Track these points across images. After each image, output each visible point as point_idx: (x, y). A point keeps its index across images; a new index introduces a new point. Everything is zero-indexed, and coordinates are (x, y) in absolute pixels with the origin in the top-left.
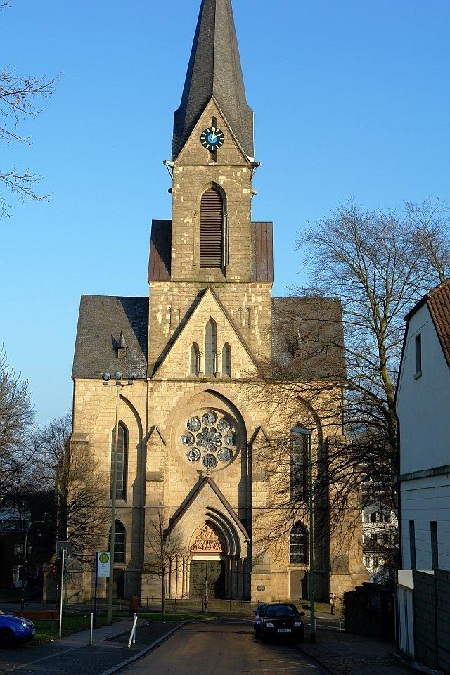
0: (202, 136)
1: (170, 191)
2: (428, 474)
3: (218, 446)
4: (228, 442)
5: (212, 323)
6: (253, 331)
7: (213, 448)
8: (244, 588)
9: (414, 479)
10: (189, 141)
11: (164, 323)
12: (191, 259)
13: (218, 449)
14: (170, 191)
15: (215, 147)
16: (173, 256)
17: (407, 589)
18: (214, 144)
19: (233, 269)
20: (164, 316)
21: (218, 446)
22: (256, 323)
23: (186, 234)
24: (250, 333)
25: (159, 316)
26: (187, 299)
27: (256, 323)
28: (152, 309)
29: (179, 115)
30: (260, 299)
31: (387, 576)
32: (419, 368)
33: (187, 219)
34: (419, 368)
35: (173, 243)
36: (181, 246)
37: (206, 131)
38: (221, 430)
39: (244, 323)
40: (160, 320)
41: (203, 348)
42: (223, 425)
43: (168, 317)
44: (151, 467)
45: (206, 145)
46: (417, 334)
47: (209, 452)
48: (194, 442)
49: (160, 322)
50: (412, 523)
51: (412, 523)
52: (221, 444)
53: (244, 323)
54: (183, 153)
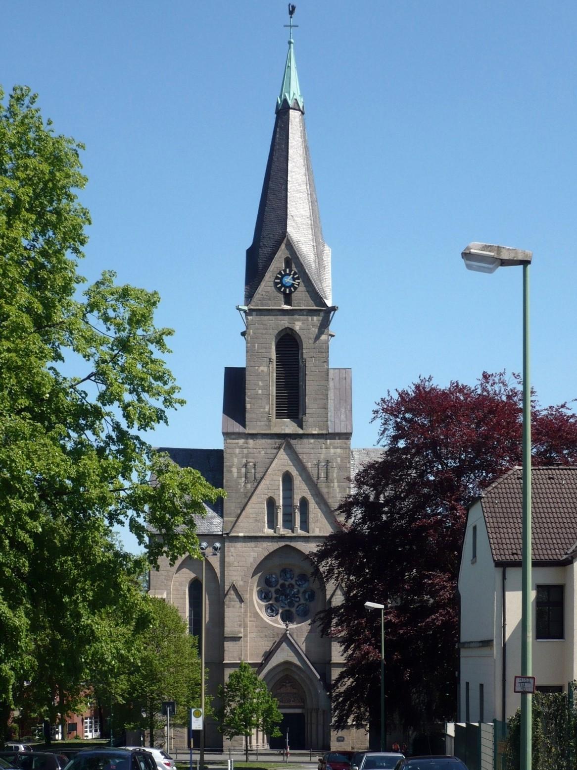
0: (277, 278)
1: (243, 334)
2: (472, 645)
3: (297, 602)
4: (307, 597)
5: (287, 479)
6: (332, 485)
7: (291, 604)
8: (325, 408)
9: (469, 647)
10: (263, 284)
11: (239, 477)
12: (267, 410)
13: (296, 604)
14: (243, 334)
15: (290, 290)
16: (248, 406)
17: (450, 736)
18: (289, 287)
19: (311, 420)
20: (239, 471)
21: (297, 602)
22: (335, 476)
23: (260, 383)
24: (328, 487)
25: (235, 470)
26: (263, 452)
27: (335, 476)
28: (226, 463)
29: (252, 254)
30: (339, 451)
31: (129, 683)
32: (475, 556)
33: (262, 368)
34: (475, 556)
35: (248, 393)
36: (256, 397)
37: (280, 273)
38: (299, 585)
39: (322, 476)
40: (233, 470)
41: (280, 502)
42: (301, 581)
43: (243, 470)
44: (230, 627)
45: (281, 288)
46: (473, 525)
47: (287, 608)
48: (272, 597)
49: (235, 475)
50: (467, 684)
51: (467, 684)
52: (300, 600)
53: (322, 476)
54: (257, 296)
